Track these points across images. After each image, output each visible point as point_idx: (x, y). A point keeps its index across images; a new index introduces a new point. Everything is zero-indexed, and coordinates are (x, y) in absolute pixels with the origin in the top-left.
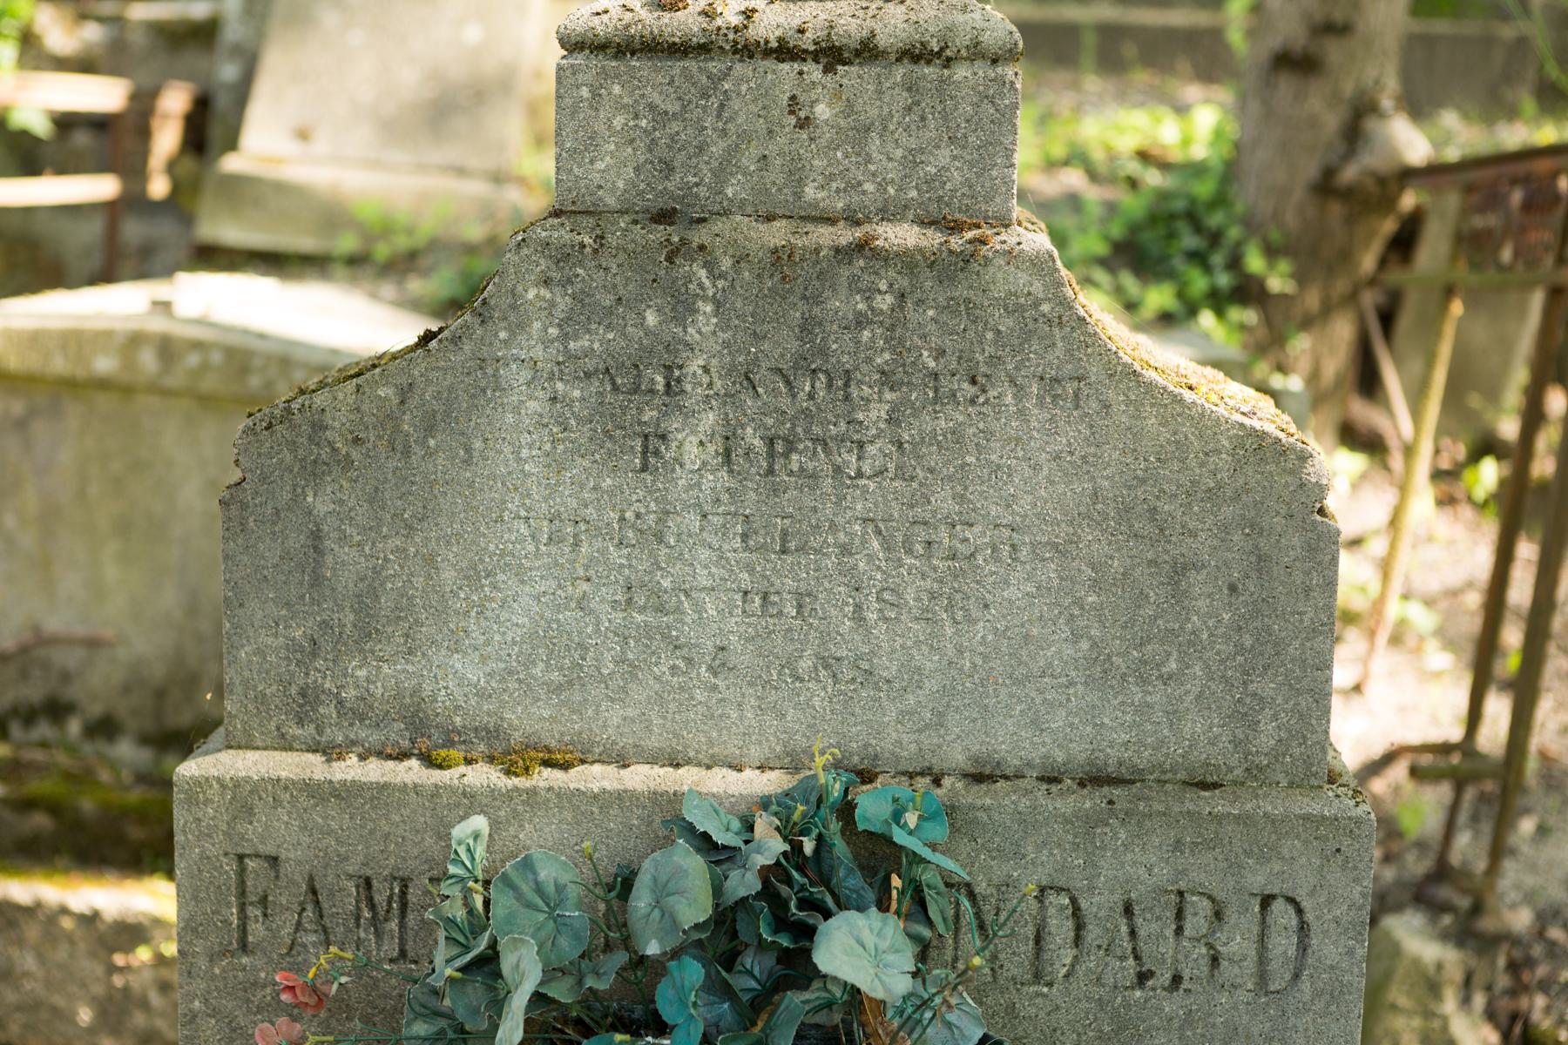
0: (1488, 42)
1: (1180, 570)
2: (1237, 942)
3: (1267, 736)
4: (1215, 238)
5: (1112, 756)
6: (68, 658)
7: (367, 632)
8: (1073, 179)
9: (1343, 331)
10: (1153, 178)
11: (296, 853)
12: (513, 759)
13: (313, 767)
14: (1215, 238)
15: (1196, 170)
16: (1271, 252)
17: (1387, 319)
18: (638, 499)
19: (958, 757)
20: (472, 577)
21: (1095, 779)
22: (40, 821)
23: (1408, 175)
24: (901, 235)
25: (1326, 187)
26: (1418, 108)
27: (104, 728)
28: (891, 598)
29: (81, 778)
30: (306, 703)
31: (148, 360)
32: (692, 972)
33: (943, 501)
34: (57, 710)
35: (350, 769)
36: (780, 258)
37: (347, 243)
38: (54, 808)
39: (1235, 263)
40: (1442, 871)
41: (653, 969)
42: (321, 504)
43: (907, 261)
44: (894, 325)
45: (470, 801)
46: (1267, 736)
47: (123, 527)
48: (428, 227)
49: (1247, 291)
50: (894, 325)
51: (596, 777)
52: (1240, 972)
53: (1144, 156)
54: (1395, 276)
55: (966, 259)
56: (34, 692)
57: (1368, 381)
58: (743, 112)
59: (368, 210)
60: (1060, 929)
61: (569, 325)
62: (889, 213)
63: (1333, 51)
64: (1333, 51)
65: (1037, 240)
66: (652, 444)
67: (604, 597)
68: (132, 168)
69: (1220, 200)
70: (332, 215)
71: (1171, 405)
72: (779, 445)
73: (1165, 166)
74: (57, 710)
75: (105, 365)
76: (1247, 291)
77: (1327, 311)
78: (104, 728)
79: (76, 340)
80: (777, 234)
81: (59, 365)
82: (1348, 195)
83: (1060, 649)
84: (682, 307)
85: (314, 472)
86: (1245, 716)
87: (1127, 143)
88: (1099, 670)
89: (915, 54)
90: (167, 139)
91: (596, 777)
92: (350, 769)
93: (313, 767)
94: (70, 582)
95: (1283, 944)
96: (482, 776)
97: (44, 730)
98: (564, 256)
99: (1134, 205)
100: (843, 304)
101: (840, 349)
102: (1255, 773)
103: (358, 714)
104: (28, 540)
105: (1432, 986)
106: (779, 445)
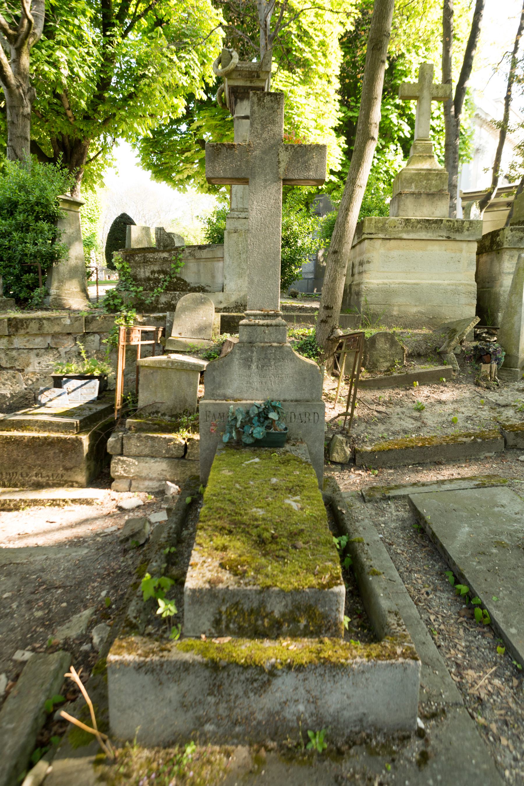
0: (354, 317)
1: (304, 379)
2: (311, 418)
3: (314, 396)
4: (313, 347)
5: (298, 398)
6: (159, 405)
7: (219, 387)
8: (293, 339)
9: (332, 359)
10: (304, 338)
11: (212, 411)
12: (235, 400)
13: (214, 401)
14: (313, 347)
15: (310, 337)
16: (321, 348)
17: (338, 358)
18: (248, 373)
19: (282, 399)
20: (231, 381)
21: (296, 401)
22: (157, 426)
23: (340, 337)
24: (275, 344)
25: (328, 339)
26: (343, 327)
27: (164, 415)
28: (275, 382)
29: (161, 421)
30: (213, 395)
31: (170, 364)
32: (256, 418)
33: (280, 372)
34: (157, 412)
35: (218, 402)
36: (263, 347)
37: (188, 350)
38: (159, 425)
39: (316, 350)
40: (344, 429)
41: (252, 419)
42: (214, 373)
43: (276, 347)
44: (274, 354)
45: (231, 404)
46: (314, 396)
47: (166, 387)
48: (200, 347)
49: (318, 354)
50: (274, 354)
51: (244, 402)
52: (312, 421)
53: (303, 335)
54: (339, 351)
55: (282, 347)
56: (154, 410)
57: (336, 367)
58: (259, 332)
59: (191, 345)
60: (293, 417)
61: (241, 354)
62: (274, 342)
63: (329, 320)
64: (329, 320)
65: (289, 345)
66: (249, 367)
67: (245, 383)
68: (155, 339)
69: (314, 341)
70: (186, 345)
71: (303, 362)
72: (263, 366)
73: (306, 336)
74: (157, 412)
75: (164, 365)
76: (318, 354)
77: (329, 357)
78: (164, 415)
79: (160, 362)
80: (262, 344)
81: (158, 365)
82: (332, 340)
83: (292, 387)
84: (252, 352)
85: (214, 370)
86: (312, 394)
87: (301, 333)
88: (297, 390)
89: (276, 326)
90: (160, 335)
91: (244, 402)
92: (218, 402)
93: (214, 401)
94: (159, 395)
95: (316, 418)
96: (232, 402)
97: (155, 415)
98: (240, 347)
99: (302, 342)
100: (269, 352)
101: (269, 356)
102: (313, 400)
103: (219, 396)
104: (153, 389)
105: (342, 443)
106: (263, 366)
